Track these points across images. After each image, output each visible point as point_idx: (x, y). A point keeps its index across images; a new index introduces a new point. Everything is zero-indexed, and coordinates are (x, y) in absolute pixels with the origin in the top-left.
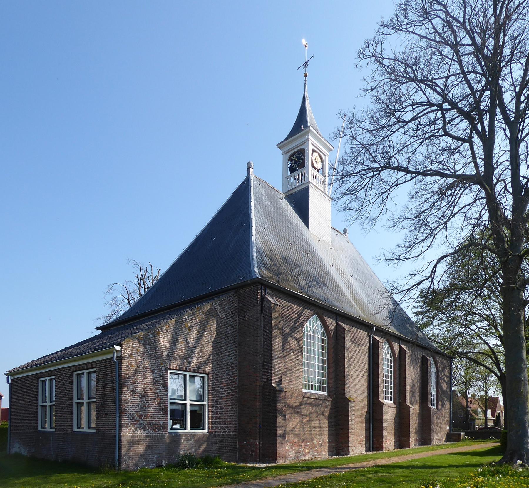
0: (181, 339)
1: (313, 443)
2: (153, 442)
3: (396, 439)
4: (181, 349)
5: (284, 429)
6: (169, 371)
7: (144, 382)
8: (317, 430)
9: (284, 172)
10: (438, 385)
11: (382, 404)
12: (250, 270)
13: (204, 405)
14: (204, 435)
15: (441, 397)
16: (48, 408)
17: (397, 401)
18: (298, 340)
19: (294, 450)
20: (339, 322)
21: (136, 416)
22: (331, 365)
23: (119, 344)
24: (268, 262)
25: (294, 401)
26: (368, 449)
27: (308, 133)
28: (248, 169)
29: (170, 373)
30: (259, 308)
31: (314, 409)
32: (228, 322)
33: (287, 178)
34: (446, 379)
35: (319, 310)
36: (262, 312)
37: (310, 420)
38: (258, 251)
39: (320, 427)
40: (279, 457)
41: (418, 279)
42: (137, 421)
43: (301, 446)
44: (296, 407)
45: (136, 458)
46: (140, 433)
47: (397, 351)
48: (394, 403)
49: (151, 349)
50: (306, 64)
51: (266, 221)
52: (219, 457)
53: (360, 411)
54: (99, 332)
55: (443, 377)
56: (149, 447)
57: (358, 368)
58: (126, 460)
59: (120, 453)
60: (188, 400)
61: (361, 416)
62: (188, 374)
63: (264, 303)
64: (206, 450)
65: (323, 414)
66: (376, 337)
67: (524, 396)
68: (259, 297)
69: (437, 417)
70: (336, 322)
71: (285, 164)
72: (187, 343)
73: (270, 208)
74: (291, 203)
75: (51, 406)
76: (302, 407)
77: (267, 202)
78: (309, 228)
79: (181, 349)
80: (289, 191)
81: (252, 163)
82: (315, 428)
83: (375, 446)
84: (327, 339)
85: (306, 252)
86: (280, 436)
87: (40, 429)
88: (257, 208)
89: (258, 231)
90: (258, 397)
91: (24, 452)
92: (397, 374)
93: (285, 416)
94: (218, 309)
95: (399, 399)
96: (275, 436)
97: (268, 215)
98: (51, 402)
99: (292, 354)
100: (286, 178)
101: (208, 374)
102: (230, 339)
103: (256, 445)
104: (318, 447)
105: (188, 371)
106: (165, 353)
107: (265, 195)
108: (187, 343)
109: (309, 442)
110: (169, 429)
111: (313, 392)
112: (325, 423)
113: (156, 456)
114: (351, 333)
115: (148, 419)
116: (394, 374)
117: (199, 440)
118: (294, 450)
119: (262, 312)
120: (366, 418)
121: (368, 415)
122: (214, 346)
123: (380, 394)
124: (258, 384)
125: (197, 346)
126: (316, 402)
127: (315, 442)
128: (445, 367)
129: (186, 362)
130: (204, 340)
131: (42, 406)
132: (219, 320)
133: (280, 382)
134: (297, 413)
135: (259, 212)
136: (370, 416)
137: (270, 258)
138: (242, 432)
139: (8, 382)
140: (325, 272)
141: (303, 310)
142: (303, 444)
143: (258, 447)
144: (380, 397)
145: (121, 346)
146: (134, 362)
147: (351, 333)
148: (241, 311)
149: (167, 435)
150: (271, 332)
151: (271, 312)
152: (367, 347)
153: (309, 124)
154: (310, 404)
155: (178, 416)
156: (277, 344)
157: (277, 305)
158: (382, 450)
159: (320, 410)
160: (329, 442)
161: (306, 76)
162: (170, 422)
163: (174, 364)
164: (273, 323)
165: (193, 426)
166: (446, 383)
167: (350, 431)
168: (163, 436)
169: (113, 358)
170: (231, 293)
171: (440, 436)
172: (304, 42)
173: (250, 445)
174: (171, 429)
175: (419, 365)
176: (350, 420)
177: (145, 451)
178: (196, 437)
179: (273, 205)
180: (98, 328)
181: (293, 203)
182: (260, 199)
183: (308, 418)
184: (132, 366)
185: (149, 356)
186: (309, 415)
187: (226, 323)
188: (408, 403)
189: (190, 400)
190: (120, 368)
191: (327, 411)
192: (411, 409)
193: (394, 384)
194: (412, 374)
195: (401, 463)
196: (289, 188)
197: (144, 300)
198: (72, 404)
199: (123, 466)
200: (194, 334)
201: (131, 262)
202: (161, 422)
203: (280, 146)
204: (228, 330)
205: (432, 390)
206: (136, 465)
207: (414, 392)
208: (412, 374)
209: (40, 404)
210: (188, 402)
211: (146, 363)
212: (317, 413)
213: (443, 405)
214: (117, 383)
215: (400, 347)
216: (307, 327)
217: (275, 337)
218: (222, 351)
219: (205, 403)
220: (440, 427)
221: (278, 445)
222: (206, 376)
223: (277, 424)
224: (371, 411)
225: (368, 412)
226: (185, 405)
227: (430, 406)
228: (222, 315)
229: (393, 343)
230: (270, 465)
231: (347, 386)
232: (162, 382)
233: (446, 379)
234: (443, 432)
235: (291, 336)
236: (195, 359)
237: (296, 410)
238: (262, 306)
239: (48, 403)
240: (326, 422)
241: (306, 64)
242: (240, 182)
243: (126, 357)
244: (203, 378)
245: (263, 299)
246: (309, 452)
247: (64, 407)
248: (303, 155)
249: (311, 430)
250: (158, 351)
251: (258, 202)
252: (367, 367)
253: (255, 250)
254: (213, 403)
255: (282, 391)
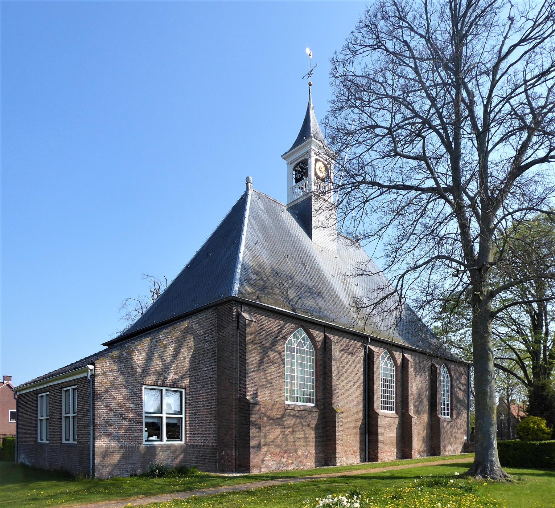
0: (156, 355)
1: (297, 454)
2: (128, 453)
3: (398, 450)
4: (157, 365)
5: (258, 441)
6: (144, 387)
7: (119, 397)
8: (302, 441)
9: (290, 182)
10: (452, 393)
11: (377, 415)
12: (231, 289)
13: (181, 418)
14: (181, 446)
15: (456, 406)
16: (71, 420)
17: (400, 411)
18: (280, 353)
19: (275, 461)
20: (325, 334)
21: (110, 429)
22: (318, 376)
23: (93, 364)
24: (254, 277)
25: (275, 413)
26: (363, 460)
27: (310, 143)
28: (247, 184)
29: (145, 388)
30: (234, 325)
31: (298, 420)
32: (207, 338)
33: (292, 188)
34: (462, 387)
35: (303, 323)
36: (238, 328)
37: (293, 431)
38: (244, 267)
39: (305, 438)
40: (254, 467)
41: (387, 292)
42: (111, 434)
43: (283, 457)
44: (277, 419)
45: (110, 468)
46: (114, 444)
47: (399, 361)
48: (396, 413)
49: (125, 367)
50: (310, 73)
51: (260, 235)
52: (195, 467)
53: (353, 422)
54: (106, 347)
55: (459, 386)
56: (123, 457)
57: (351, 379)
58: (99, 470)
59: (94, 463)
60: (164, 412)
61: (355, 428)
62: (164, 389)
63: (240, 320)
64: (182, 461)
65: (309, 425)
66: (372, 347)
67: (490, 408)
68: (235, 313)
69: (451, 426)
70: (324, 334)
71: (290, 175)
72: (163, 360)
73: (267, 222)
74: (293, 214)
75: (74, 417)
76: (284, 419)
77: (265, 216)
78: (311, 239)
79: (157, 365)
80: (293, 202)
81: (251, 178)
82: (299, 439)
83: (371, 457)
84: (314, 351)
85: (303, 264)
86: (254, 447)
87: (64, 441)
88: (251, 223)
89: (247, 247)
90: (234, 410)
91: (27, 462)
92: (399, 383)
93: (260, 428)
94: (196, 326)
95: (402, 410)
96: (249, 447)
97: (263, 228)
98: (74, 413)
99: (273, 367)
100: (291, 189)
101: (185, 389)
102: (209, 354)
103: (232, 455)
104: (303, 458)
105: (162, 385)
106: (139, 370)
107: (263, 209)
108: (163, 360)
109: (292, 453)
110: (144, 441)
111: (299, 403)
112: (311, 435)
113: (130, 466)
114: (338, 345)
115: (122, 431)
116: (396, 384)
117: (174, 451)
118: (275, 461)
119: (238, 328)
120: (360, 428)
121: (363, 426)
122: (192, 361)
123: (375, 405)
124: (234, 397)
125: (173, 362)
126: (300, 414)
127: (299, 453)
128: (461, 375)
129: (161, 378)
130: (181, 356)
131: (66, 417)
132: (196, 337)
133: (255, 395)
134: (279, 424)
135: (253, 227)
136: (365, 427)
137: (257, 273)
138: (221, 443)
139: (15, 398)
140: (323, 283)
141: (285, 324)
142: (286, 455)
143: (234, 457)
144: (375, 407)
145: (94, 365)
146: (108, 380)
147: (338, 345)
148: (220, 327)
149: (141, 447)
150: (245, 347)
151: (245, 328)
152: (362, 358)
153: (312, 135)
154: (294, 416)
155: (154, 428)
156: (253, 358)
157: (252, 321)
158: (377, 461)
159: (305, 421)
160: (316, 453)
161: (310, 85)
162: (145, 435)
163: (151, 379)
164: (248, 338)
165: (169, 438)
166: (463, 391)
167: (337, 442)
168: (138, 448)
169: (86, 377)
170: (210, 311)
171: (455, 446)
172: (308, 51)
173: (228, 455)
174: (146, 441)
175: (427, 374)
176: (337, 431)
177: (120, 461)
178: (172, 448)
179: (272, 218)
180: (104, 344)
181: (297, 214)
182: (257, 214)
183: (291, 430)
184: (106, 383)
185: (123, 373)
186: (293, 426)
187: (205, 339)
188: (411, 412)
189: (167, 414)
190: (93, 385)
191: (314, 423)
192: (413, 419)
193: (396, 394)
194: (417, 384)
195: (368, 474)
196: (294, 198)
197: (145, 317)
198: (61, 418)
199: (96, 474)
200: (170, 351)
201: (145, 277)
202: (136, 434)
203: (285, 156)
204: (207, 346)
205: (444, 398)
206: (110, 473)
207: (421, 402)
208: (417, 384)
209: (64, 415)
210: (164, 416)
211: (121, 380)
212: (302, 425)
213: (458, 415)
214: (91, 400)
215: (403, 356)
216: (291, 340)
217: (251, 351)
218: (200, 366)
219: (183, 416)
220: (455, 437)
221: (251, 456)
222: (183, 390)
223: (251, 435)
224: (367, 422)
225: (364, 423)
226: (162, 418)
227: (440, 416)
228: (200, 332)
229: (395, 353)
230: (243, 475)
231: (334, 398)
232: (137, 398)
233: (462, 387)
234: (458, 442)
235: (272, 350)
236: (171, 374)
237: (278, 421)
238: (238, 322)
239: (71, 414)
240: (313, 433)
241: (310, 73)
242: (239, 198)
243: (99, 375)
244: (181, 392)
245: (239, 316)
246: (292, 463)
247: (55, 422)
248: (306, 165)
249: (294, 442)
250: (132, 368)
251: (253, 217)
252: (362, 377)
253: (239, 266)
254: (192, 415)
255: (256, 403)
